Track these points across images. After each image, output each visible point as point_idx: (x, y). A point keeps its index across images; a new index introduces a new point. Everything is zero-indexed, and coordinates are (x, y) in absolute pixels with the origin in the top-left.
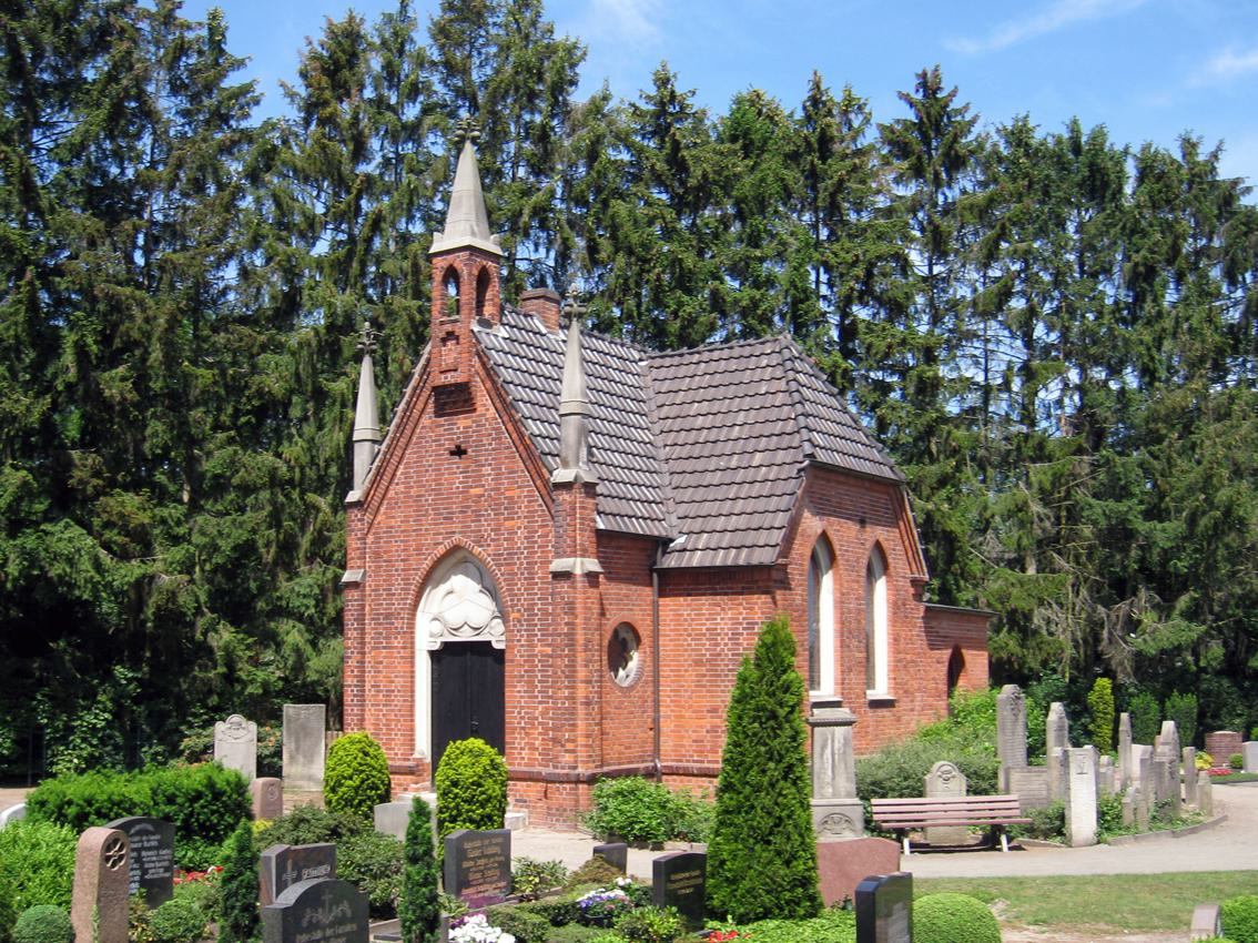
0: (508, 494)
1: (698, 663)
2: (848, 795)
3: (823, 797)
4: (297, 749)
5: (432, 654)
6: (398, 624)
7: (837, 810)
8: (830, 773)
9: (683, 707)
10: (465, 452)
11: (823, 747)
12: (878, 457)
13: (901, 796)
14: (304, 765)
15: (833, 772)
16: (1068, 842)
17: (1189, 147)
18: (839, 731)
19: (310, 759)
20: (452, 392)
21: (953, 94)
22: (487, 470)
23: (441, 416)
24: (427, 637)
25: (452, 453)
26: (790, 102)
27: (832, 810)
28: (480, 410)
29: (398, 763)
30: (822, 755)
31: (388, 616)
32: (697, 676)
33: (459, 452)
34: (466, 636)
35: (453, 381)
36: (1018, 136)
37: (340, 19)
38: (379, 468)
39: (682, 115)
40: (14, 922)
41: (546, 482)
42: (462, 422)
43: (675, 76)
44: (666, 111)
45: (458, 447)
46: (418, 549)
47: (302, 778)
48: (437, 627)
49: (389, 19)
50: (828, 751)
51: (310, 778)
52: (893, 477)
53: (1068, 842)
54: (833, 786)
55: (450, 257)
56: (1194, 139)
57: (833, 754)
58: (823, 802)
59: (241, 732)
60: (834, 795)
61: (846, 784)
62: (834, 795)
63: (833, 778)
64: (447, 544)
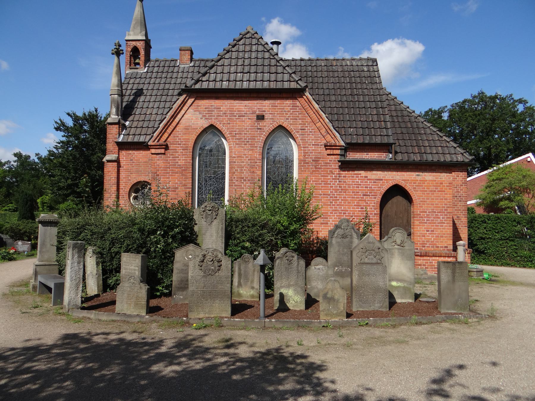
55: (137, 42)
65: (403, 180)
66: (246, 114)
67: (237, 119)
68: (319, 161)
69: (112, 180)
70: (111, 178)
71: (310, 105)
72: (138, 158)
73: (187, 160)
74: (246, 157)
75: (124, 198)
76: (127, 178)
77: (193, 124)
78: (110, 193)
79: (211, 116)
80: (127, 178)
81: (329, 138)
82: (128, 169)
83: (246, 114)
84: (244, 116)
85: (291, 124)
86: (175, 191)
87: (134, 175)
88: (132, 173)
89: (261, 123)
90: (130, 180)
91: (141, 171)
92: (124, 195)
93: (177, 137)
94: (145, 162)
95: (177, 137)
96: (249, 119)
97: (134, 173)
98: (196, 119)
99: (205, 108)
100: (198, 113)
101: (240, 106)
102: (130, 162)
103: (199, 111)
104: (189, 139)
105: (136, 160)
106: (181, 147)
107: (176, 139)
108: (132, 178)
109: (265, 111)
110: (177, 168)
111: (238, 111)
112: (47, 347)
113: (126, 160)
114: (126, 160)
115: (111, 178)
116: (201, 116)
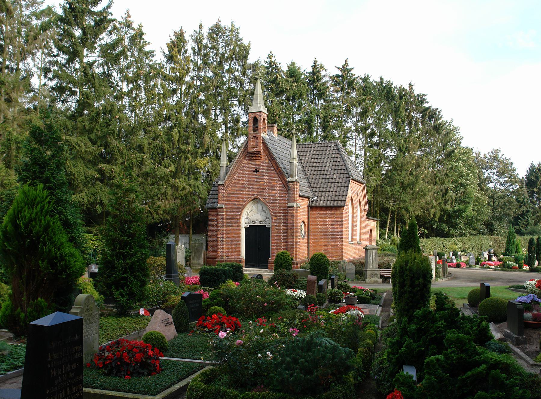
0: (273, 184)
1: (321, 232)
2: (376, 268)
4: (195, 256)
6: (236, 220)
7: (374, 272)
10: (259, 171)
11: (370, 255)
13: (385, 268)
14: (197, 260)
17: (411, 86)
18: (374, 251)
19: (199, 259)
20: (255, 154)
22: (266, 177)
23: (251, 160)
24: (244, 223)
25: (254, 171)
26: (306, 67)
28: (264, 159)
29: (236, 260)
31: (232, 218)
33: (256, 171)
34: (257, 224)
35: (256, 150)
36: (366, 80)
39: (276, 68)
42: (258, 163)
44: (272, 66)
45: (256, 170)
46: (243, 199)
47: (196, 264)
48: (247, 221)
50: (371, 256)
51: (199, 264)
56: (412, 84)
60: (373, 268)
61: (376, 265)
64: (300, 198)
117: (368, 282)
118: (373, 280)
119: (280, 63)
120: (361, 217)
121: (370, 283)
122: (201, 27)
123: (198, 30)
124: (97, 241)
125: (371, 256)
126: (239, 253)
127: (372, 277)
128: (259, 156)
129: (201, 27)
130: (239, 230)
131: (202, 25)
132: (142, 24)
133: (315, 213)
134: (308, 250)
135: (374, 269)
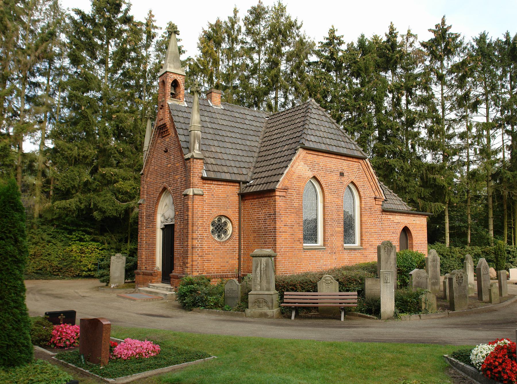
1: (254, 232)
3: (256, 290)
5: (162, 229)
7: (261, 296)
8: (259, 279)
9: (250, 250)
11: (256, 267)
12: (354, 147)
13: (309, 291)
15: (260, 279)
16: (380, 318)
18: (264, 260)
20: (163, 128)
21: (450, 27)
27: (258, 296)
30: (256, 271)
32: (254, 237)
37: (213, 22)
38: (147, 160)
40: (421, 308)
41: (183, 158)
43: (337, 30)
49: (230, 19)
50: (259, 269)
52: (362, 155)
53: (380, 318)
54: (260, 286)
55: (177, 76)
57: (261, 270)
58: (255, 292)
59: (120, 260)
60: (261, 290)
62: (261, 290)
63: (261, 282)
65: (408, 223)
66: (334, 170)
67: (329, 173)
68: (371, 209)
69: (199, 213)
70: (198, 211)
71: (368, 169)
72: (218, 193)
73: (299, 203)
74: (335, 203)
75: (206, 230)
76: (209, 212)
77: (303, 174)
78: (197, 226)
79: (314, 169)
80: (209, 212)
81: (377, 194)
82: (210, 203)
83: (334, 170)
84: (333, 172)
85: (358, 181)
86: (292, 228)
87: (215, 210)
88: (213, 208)
89: (343, 179)
90: (211, 214)
91: (221, 206)
92: (206, 228)
93: (293, 183)
94: (224, 198)
95: (293, 183)
96: (336, 174)
97: (215, 208)
98: (305, 170)
99: (311, 163)
100: (306, 165)
101: (330, 164)
102: (212, 197)
103: (307, 164)
104: (300, 186)
105: (216, 195)
106: (296, 192)
107: (292, 185)
108: (213, 212)
109: (344, 170)
110: (293, 209)
111: (330, 168)
112: (478, 329)
113: (208, 195)
114: (208, 195)
115: (198, 211)
116: (308, 168)
117: (249, 315)
118: (258, 311)
119: (343, 36)
120: (361, 208)
121: (252, 316)
122: (236, 11)
123: (232, 15)
124: (105, 251)
125: (259, 269)
126: (154, 263)
127: (259, 307)
128: (167, 131)
129: (236, 11)
130: (154, 232)
131: (237, 10)
132: (175, 23)
133: (248, 203)
134: (239, 259)
135: (261, 292)
